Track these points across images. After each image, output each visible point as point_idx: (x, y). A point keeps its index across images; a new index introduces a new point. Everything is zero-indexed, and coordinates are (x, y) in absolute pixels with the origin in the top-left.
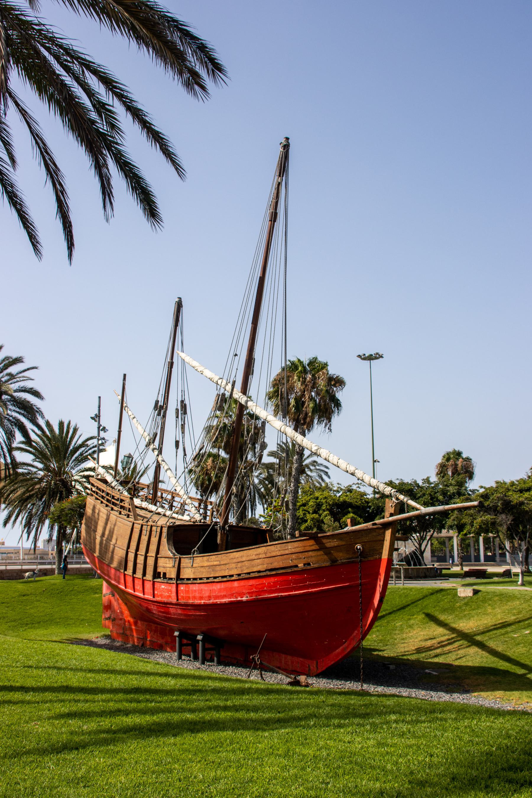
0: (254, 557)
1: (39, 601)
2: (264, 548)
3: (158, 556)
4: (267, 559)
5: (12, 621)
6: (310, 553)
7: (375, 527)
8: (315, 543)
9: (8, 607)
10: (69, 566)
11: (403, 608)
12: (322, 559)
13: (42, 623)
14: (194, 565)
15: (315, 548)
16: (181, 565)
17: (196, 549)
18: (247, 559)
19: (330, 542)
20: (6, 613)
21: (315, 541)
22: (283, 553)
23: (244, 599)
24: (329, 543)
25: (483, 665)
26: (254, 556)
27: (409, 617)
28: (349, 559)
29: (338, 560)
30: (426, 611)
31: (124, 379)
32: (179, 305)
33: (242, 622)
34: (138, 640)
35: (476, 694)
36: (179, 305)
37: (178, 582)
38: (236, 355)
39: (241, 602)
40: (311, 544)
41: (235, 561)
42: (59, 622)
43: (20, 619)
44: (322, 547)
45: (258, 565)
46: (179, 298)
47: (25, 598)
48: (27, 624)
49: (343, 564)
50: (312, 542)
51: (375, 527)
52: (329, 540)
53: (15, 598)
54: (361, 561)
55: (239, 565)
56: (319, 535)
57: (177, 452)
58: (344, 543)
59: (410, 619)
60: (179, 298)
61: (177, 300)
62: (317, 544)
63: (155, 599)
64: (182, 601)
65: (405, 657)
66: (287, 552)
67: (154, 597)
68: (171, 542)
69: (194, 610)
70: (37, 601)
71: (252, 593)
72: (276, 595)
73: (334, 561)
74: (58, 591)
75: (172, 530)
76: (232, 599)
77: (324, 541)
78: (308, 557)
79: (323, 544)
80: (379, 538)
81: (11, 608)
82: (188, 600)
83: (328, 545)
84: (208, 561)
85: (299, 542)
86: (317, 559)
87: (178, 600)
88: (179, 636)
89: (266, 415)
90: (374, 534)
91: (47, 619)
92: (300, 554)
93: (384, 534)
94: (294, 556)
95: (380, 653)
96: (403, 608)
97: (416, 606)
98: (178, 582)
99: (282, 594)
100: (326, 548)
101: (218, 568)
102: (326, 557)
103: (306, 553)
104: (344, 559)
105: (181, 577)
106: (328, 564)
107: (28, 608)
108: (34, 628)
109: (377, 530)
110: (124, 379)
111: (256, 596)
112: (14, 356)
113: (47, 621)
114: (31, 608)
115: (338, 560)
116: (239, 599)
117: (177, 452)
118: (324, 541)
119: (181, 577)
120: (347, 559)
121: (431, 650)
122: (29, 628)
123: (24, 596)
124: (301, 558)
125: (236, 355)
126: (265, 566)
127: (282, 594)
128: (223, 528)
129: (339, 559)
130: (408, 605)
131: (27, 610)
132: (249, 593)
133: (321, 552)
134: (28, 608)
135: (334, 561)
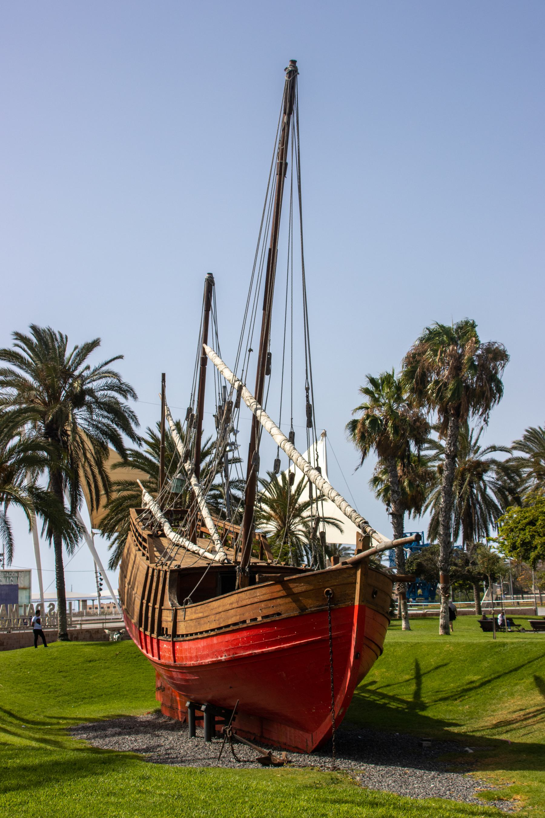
0: (228, 607)
1: (108, 668)
2: (236, 595)
3: (163, 608)
4: (239, 609)
5: (65, 695)
6: (279, 600)
7: (345, 566)
8: (282, 589)
9: (65, 677)
10: (409, 612)
11: (516, 670)
12: (290, 607)
13: (104, 696)
14: (187, 618)
15: (282, 595)
16: (178, 618)
17: (188, 598)
18: (223, 610)
19: (297, 586)
20: (60, 685)
21: (282, 586)
22: (253, 602)
23: (223, 658)
24: (298, 588)
25: (535, 742)
26: (228, 605)
27: (516, 682)
28: (320, 606)
29: (307, 609)
30: (537, 674)
31: (164, 380)
32: (210, 283)
33: (231, 687)
34: (182, 715)
35: (471, 773)
36: (210, 283)
37: (175, 639)
38: (251, 350)
39: (220, 662)
40: (278, 589)
41: (214, 612)
42: (127, 695)
43: (77, 692)
44: (290, 594)
45: (232, 617)
46: (209, 274)
47: (90, 664)
48: (84, 698)
49: (312, 613)
50: (278, 587)
51: (345, 566)
52: (296, 585)
53: (78, 664)
54: (331, 609)
55: (218, 616)
56: (285, 579)
57: (278, 455)
58: (312, 588)
59: (516, 684)
60: (209, 274)
61: (207, 276)
62: (284, 589)
63: (159, 662)
64: (178, 663)
65: (478, 734)
66: (256, 600)
67: (159, 659)
68: (174, 591)
69: (189, 673)
70: (105, 668)
71: (229, 650)
72: (250, 652)
73: (303, 609)
74: (135, 655)
75: (176, 575)
76: (214, 659)
77: (291, 585)
78: (277, 606)
79: (290, 589)
80: (350, 580)
81: (68, 678)
82: (182, 661)
83: (296, 590)
84: (195, 613)
85: (267, 588)
86: (286, 608)
87: (175, 661)
88: (190, 706)
89: (270, 427)
90: (345, 575)
91: (112, 691)
92: (268, 602)
93: (355, 574)
94: (263, 605)
95: (455, 730)
96: (516, 670)
97: (529, 667)
98: (175, 639)
99: (256, 651)
100: (294, 594)
101: (202, 621)
102: (294, 605)
103: (274, 601)
104: (314, 607)
105: (178, 633)
106: (296, 613)
107: (91, 677)
108: (92, 703)
109: (348, 571)
110: (164, 380)
111: (233, 654)
112: (90, 341)
113: (111, 694)
114: (96, 678)
115: (307, 609)
116: (220, 658)
117: (278, 455)
118: (291, 585)
119: (178, 633)
120: (317, 607)
121: (513, 724)
122: (85, 704)
123: (90, 661)
124: (269, 607)
125: (251, 350)
126: (238, 617)
127: (256, 651)
128: (243, 569)
129: (308, 607)
130: (523, 666)
131: (90, 679)
132: (226, 650)
133: (289, 600)
134: (91, 677)
135: (303, 609)
